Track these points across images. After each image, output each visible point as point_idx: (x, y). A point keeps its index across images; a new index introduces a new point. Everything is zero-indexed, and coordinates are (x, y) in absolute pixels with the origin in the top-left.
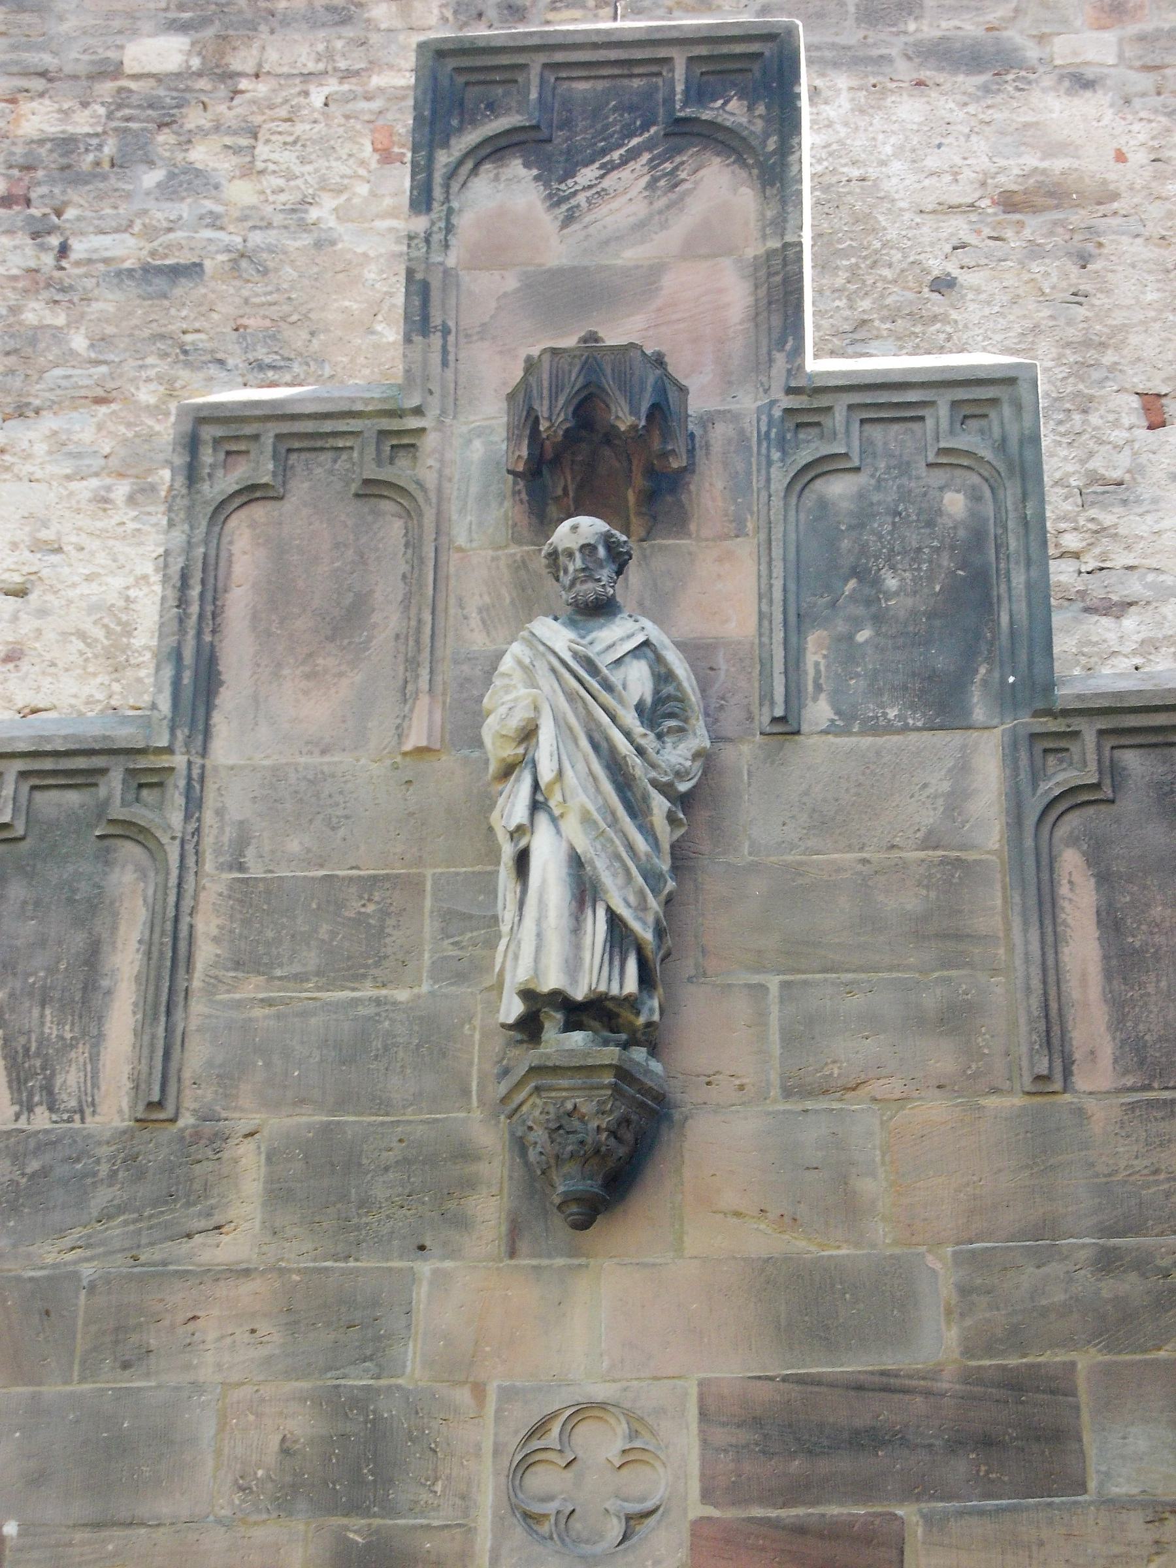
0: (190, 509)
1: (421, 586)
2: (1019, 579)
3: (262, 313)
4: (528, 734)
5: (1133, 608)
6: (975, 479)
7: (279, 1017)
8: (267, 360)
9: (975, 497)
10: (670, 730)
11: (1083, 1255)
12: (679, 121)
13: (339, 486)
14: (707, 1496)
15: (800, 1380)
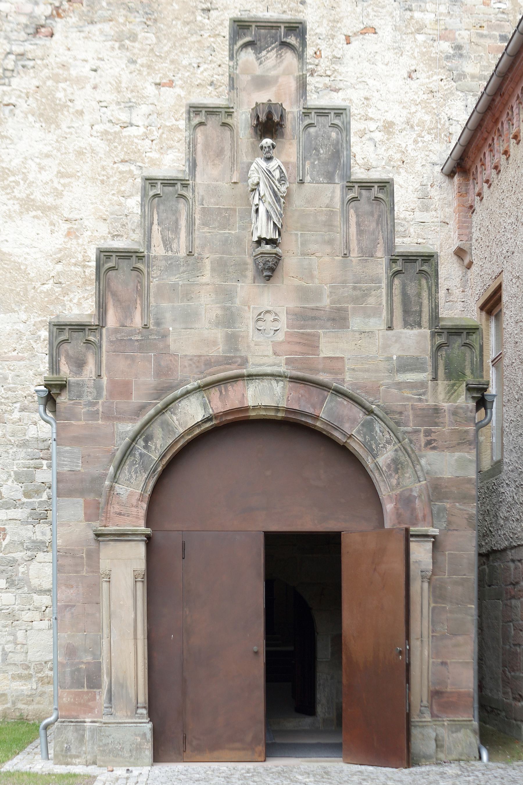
0: (189, 128)
1: (234, 147)
2: (345, 153)
3: (261, 176)
4: (258, 184)
5: (341, 91)
6: (337, 130)
7: (211, 235)
8: (148, 12)
9: (337, 134)
10: (283, 184)
11: (351, 287)
12: (282, 42)
13: (217, 123)
14: (287, 327)
15: (303, 307)
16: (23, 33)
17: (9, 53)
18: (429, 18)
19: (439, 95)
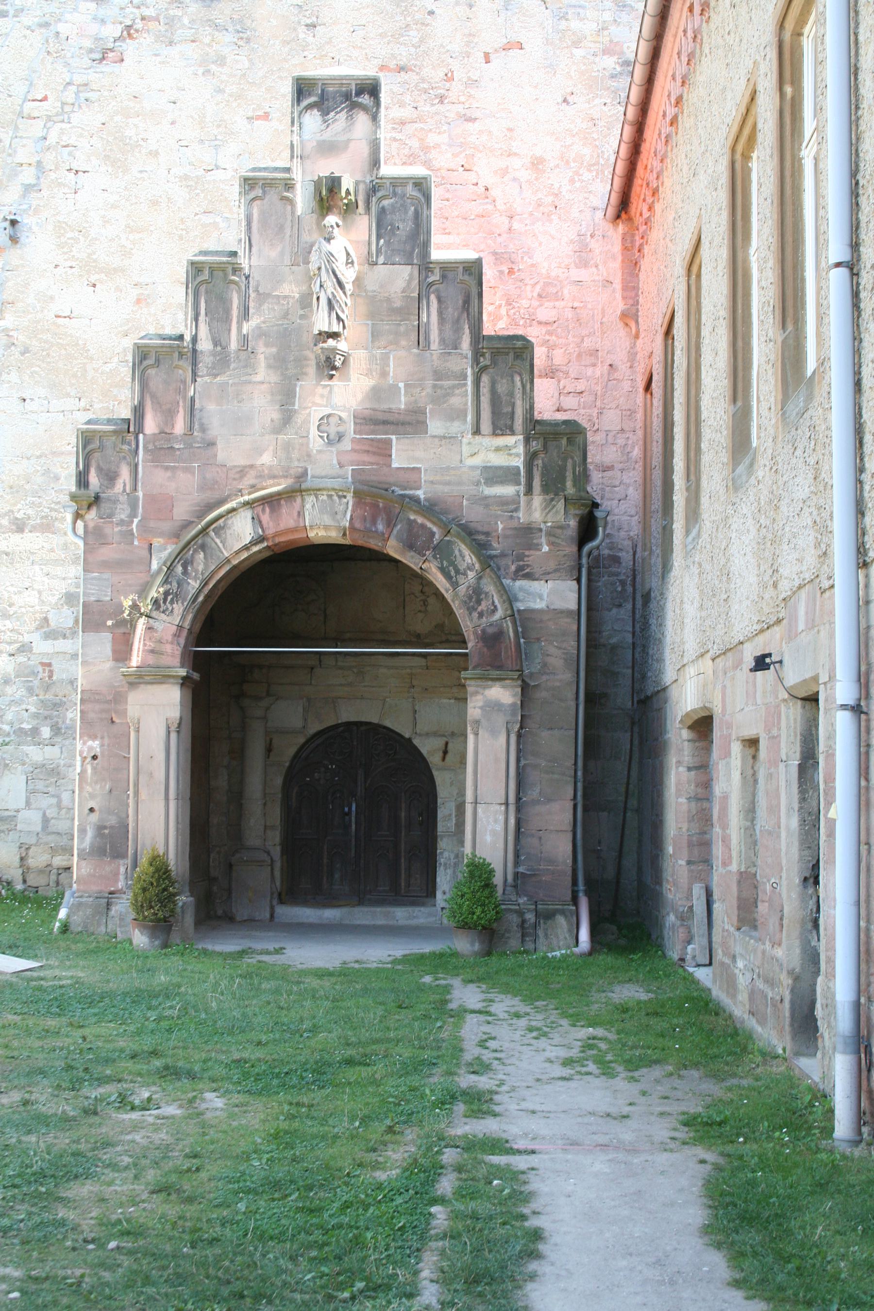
16: (86, 59)
17: (68, 84)
18: (589, 27)
19: (602, 123)
